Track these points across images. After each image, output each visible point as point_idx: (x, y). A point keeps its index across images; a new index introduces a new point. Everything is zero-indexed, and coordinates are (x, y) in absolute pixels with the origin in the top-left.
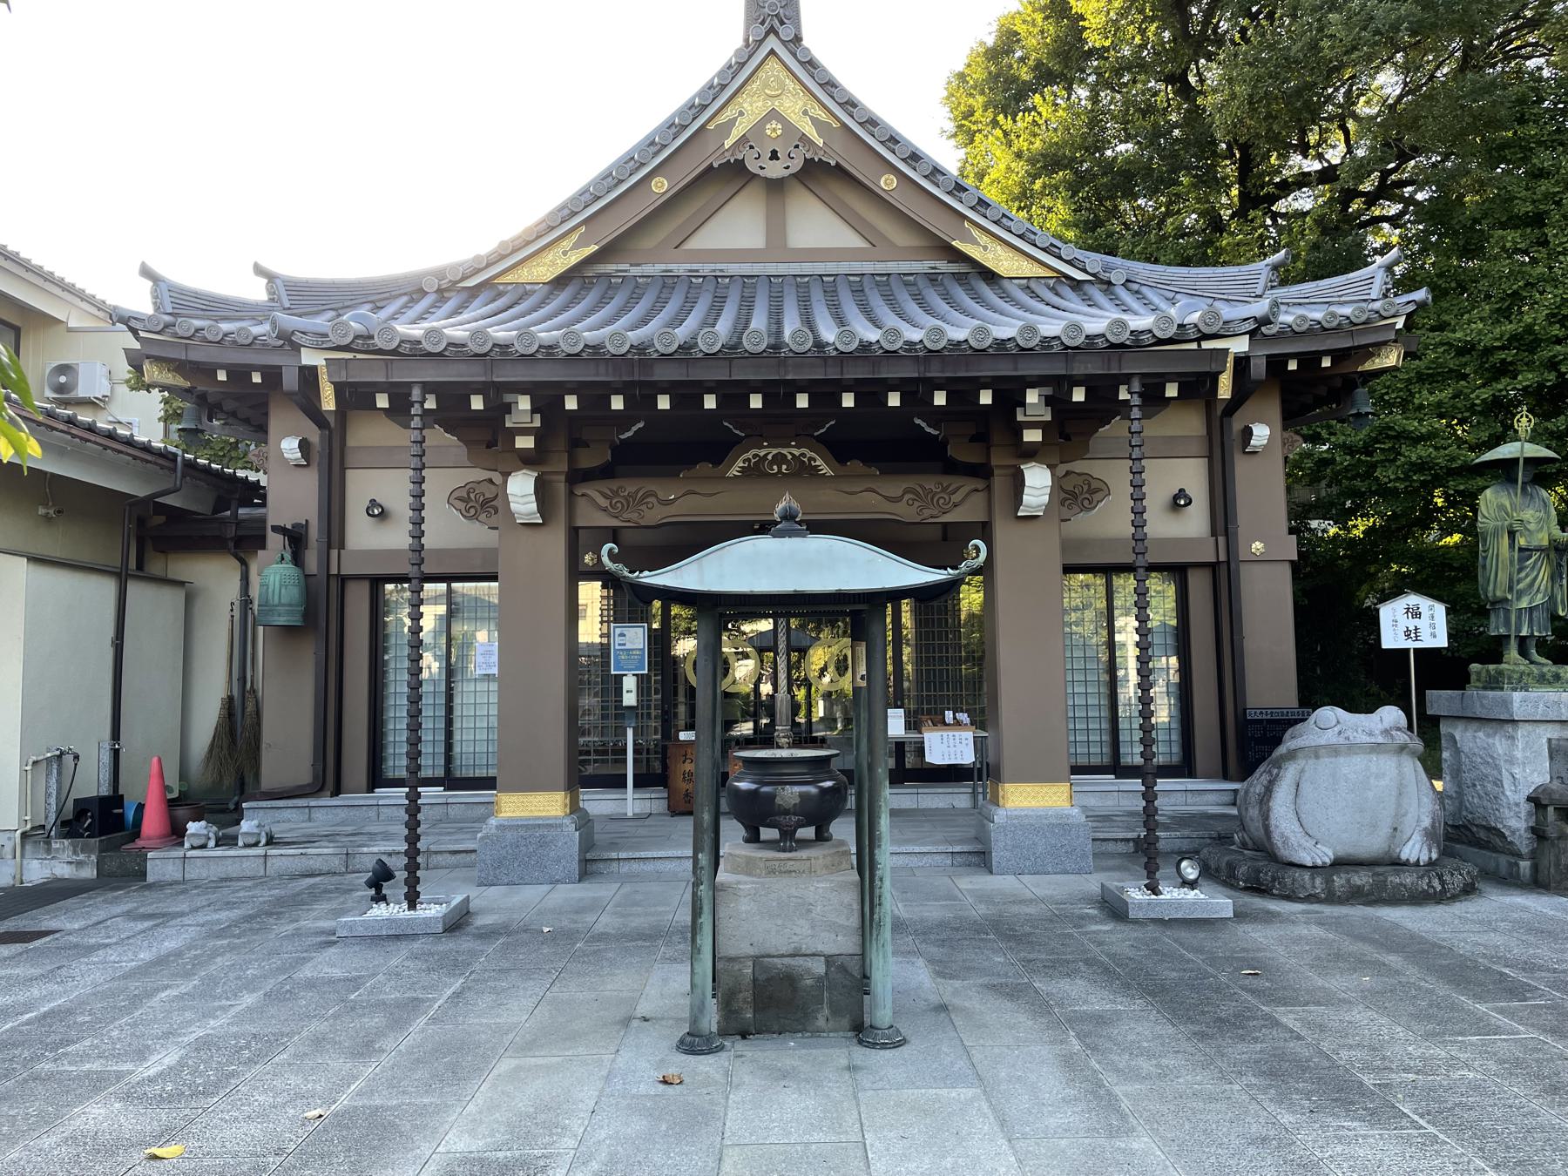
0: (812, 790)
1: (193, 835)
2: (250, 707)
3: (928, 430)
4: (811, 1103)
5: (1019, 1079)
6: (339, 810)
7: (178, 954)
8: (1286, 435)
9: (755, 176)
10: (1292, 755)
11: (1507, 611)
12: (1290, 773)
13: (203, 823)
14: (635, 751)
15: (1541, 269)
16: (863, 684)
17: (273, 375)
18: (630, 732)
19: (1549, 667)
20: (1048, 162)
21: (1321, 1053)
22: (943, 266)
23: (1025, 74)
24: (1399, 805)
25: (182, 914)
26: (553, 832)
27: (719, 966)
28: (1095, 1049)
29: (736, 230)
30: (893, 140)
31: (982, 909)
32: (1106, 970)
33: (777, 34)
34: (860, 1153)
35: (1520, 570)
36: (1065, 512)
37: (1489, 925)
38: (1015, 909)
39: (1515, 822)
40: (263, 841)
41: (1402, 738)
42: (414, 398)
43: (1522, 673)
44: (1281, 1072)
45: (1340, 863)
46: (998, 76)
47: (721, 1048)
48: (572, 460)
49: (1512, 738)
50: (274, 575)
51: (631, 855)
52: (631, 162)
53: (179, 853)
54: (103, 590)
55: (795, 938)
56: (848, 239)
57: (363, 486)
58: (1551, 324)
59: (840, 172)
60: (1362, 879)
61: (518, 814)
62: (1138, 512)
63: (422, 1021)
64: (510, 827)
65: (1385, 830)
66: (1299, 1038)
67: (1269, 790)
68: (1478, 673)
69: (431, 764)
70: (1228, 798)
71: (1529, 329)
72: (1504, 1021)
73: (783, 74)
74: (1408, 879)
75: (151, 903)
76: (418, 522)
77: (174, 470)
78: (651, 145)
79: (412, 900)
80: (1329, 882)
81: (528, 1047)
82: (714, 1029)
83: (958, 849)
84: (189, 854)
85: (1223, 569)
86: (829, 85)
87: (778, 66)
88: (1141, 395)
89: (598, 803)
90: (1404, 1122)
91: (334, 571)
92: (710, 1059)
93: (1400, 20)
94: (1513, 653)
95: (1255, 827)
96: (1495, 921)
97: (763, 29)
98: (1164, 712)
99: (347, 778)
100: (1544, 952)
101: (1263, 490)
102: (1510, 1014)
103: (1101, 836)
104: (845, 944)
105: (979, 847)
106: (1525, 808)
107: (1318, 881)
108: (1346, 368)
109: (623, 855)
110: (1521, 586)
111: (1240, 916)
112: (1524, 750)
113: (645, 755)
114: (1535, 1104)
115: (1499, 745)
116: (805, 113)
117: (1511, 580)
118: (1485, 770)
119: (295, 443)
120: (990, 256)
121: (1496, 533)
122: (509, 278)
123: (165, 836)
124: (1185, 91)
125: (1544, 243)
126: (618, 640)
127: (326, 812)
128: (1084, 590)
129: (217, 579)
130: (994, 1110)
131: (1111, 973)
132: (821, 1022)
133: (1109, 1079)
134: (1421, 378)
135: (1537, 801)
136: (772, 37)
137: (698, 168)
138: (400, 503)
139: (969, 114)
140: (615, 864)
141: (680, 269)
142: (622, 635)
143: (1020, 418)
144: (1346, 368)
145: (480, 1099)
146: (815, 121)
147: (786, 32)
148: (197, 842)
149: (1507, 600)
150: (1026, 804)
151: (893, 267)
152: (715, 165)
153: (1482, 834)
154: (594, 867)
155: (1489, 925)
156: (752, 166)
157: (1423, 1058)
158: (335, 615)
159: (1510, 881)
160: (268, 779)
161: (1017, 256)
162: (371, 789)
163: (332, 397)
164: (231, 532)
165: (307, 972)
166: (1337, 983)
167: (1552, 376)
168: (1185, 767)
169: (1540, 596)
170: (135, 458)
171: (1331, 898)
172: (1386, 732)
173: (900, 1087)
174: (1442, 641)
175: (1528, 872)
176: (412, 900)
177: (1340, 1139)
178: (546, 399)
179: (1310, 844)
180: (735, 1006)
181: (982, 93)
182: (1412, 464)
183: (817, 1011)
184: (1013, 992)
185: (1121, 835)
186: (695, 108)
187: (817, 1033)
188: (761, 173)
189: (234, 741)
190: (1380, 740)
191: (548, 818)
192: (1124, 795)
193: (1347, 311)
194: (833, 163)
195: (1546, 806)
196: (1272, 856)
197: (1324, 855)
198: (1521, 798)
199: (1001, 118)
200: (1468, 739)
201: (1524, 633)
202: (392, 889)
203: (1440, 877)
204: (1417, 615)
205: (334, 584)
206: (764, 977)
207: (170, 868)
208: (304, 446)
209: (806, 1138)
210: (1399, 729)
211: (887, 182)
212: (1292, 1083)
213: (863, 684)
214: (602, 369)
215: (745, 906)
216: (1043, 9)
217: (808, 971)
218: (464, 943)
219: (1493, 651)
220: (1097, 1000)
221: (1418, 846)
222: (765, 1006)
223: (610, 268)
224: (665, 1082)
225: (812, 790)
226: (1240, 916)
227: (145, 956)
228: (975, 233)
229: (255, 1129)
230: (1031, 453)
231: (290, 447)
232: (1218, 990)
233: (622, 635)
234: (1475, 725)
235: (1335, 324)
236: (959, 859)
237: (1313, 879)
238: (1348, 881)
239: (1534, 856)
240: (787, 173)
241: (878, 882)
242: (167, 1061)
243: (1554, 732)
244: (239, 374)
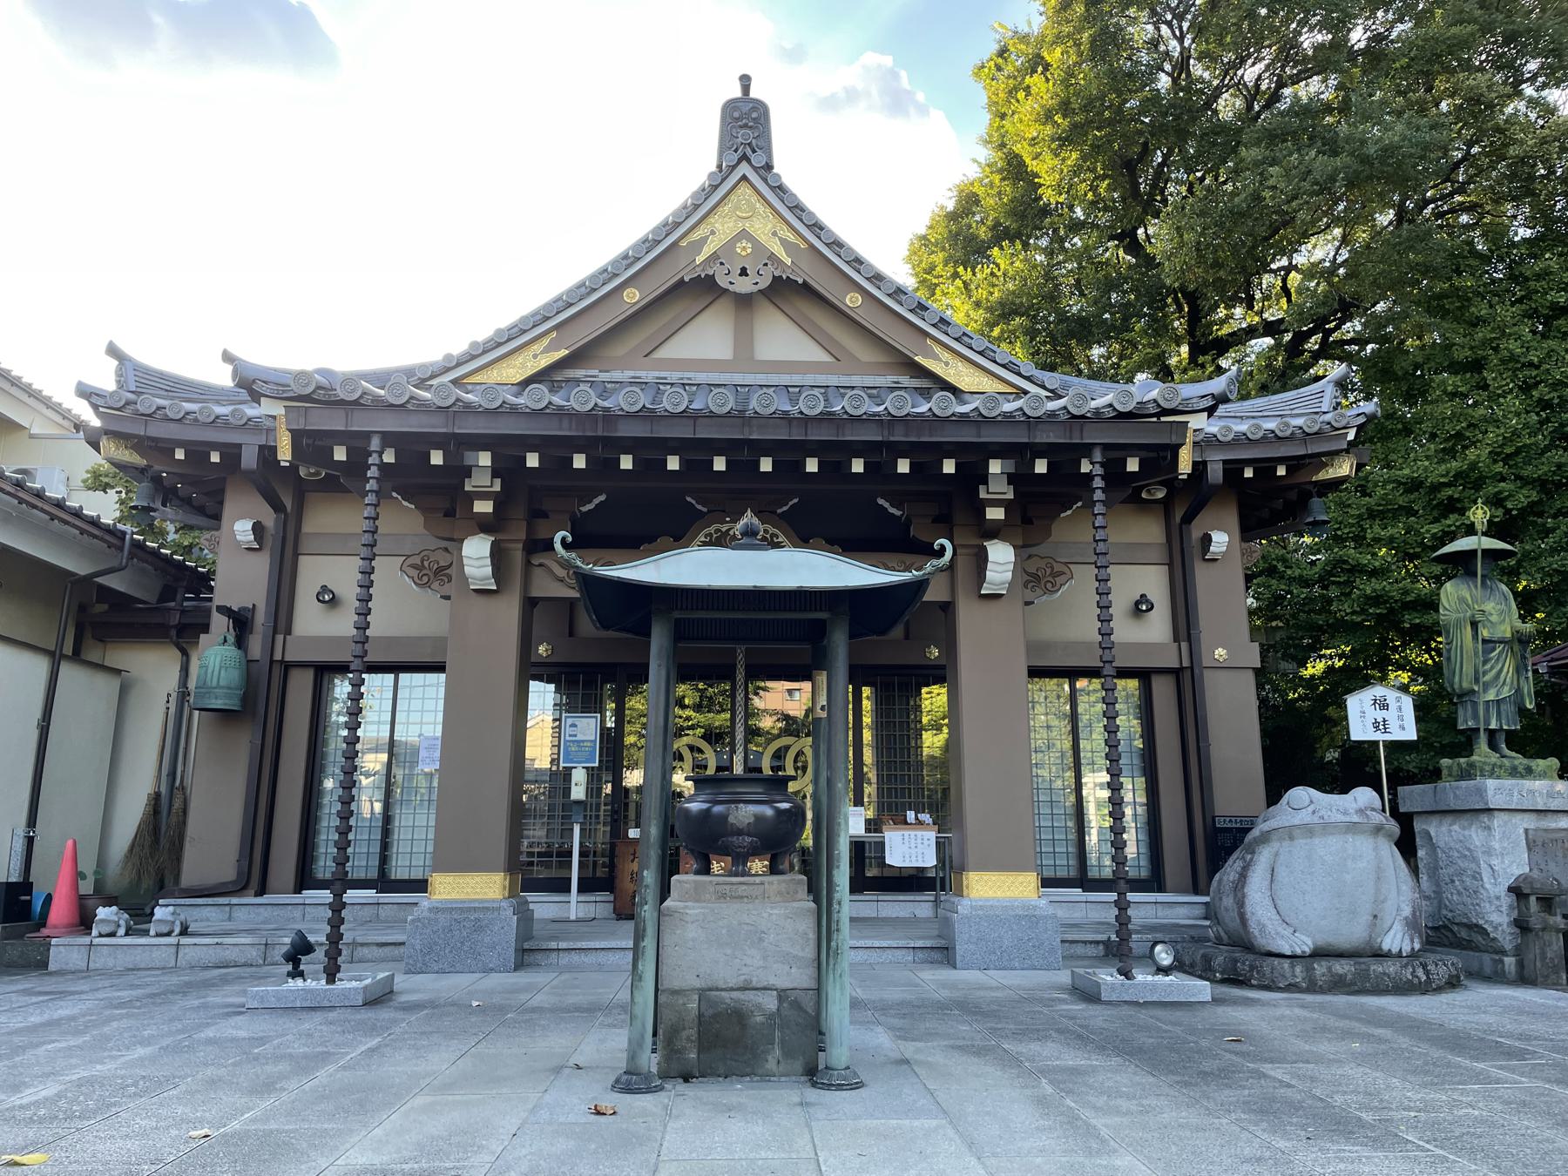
0: (768, 811)
1: (102, 921)
2: (177, 804)
3: (892, 510)
4: (758, 1129)
5: (988, 1113)
6: (262, 909)
7: (73, 1018)
8: (1245, 545)
9: (727, 290)
10: (1265, 838)
11: (1475, 704)
12: (1264, 856)
13: (114, 908)
14: (581, 855)
15: (1481, 411)
16: (824, 715)
17: (232, 454)
18: (577, 829)
19: (1520, 760)
20: (1005, 311)
21: (1314, 1097)
22: (906, 381)
23: (983, 233)
24: (1378, 890)
25: (82, 992)
26: (489, 915)
27: (662, 999)
28: (1069, 1092)
29: (704, 342)
30: (857, 262)
31: (945, 993)
32: (1080, 1037)
33: (749, 161)
34: (813, 1166)
35: (1485, 663)
36: (1029, 596)
37: (1479, 1009)
38: (982, 993)
39: (1497, 916)
40: (177, 930)
41: (1378, 818)
42: (373, 448)
43: (1494, 765)
44: (1270, 1110)
45: (1319, 954)
46: (958, 234)
47: (660, 1089)
48: (530, 529)
49: (1489, 828)
50: (216, 658)
51: (571, 945)
52: (606, 274)
53: (86, 940)
54: (38, 667)
55: (745, 970)
56: (811, 352)
57: (314, 572)
58: (1495, 462)
59: (807, 290)
60: (1342, 967)
61: (454, 896)
62: (1105, 619)
63: (331, 1068)
64: (444, 910)
65: (1365, 918)
66: (1289, 1086)
67: (1243, 876)
68: (1450, 768)
69: (362, 862)
70: (1200, 911)
71: (1473, 466)
72: (1503, 1074)
73: (755, 198)
74: (1391, 968)
75: (49, 984)
76: (365, 613)
77: (121, 549)
78: (626, 259)
79: (331, 974)
80: (1309, 970)
81: (447, 1087)
82: (654, 1070)
83: (920, 944)
84: (96, 941)
85: (1188, 674)
86: (798, 208)
87: (749, 191)
88: (1102, 465)
89: (544, 906)
90: (1409, 1146)
91: (278, 657)
92: (648, 1097)
93: (1336, 171)
94: (1482, 744)
95: (1231, 919)
96: (1482, 1006)
97: (736, 156)
98: (1133, 846)
99: (272, 880)
100: (1539, 1027)
101: (1227, 602)
102: (1512, 1070)
103: (1069, 937)
104: (798, 977)
105: (942, 943)
106: (1507, 900)
107: (1298, 969)
108: (1301, 478)
109: (563, 945)
110: (1487, 678)
111: (1216, 1001)
112: (1501, 840)
113: (591, 858)
114: (1548, 1133)
115: (1474, 835)
116: (774, 234)
117: (1476, 672)
118: (1462, 864)
119: (248, 525)
120: (952, 372)
121: (1459, 624)
122: (476, 379)
123: (73, 925)
124: (1134, 247)
125: (1485, 387)
126: (569, 731)
127: (249, 910)
128: (1048, 697)
129: (155, 671)
130: (961, 1136)
131: (1081, 1038)
132: (771, 1064)
133: (1086, 1114)
134: (1372, 514)
135: (1518, 892)
136: (744, 163)
137: (670, 283)
138: (348, 590)
139: (930, 269)
140: (554, 955)
141: (649, 376)
142: (573, 725)
143: (983, 495)
144: (1301, 478)
145: (387, 1125)
146: (784, 242)
147: (758, 159)
148: (106, 929)
149: (1473, 691)
150: (991, 894)
151: (856, 380)
152: (687, 279)
153: (1464, 934)
154: (528, 958)
155: (1479, 1009)
156: (722, 282)
157: (1422, 1100)
158: (277, 709)
159: (1496, 977)
160: (188, 878)
161: (978, 373)
162: (298, 890)
163: (289, 447)
164: (175, 619)
165: (210, 1033)
166: (1325, 1047)
167: (1500, 512)
168: (1155, 882)
169: (1506, 688)
170: (82, 532)
171: (1312, 988)
172: (1361, 811)
173: (856, 1118)
174: (1411, 734)
175: (1513, 968)
176: (331, 974)
177: (1342, 1160)
178: (507, 452)
179: (1287, 932)
180: (678, 1045)
181: (943, 249)
182: (1367, 597)
183: (767, 1052)
184: (980, 1052)
185: (1090, 937)
186: (669, 227)
187: (766, 1076)
188: (731, 288)
189: (156, 841)
190: (1356, 819)
191: (482, 901)
192: (1097, 909)
193: (1299, 422)
194: (800, 281)
195: (1527, 895)
196: (1248, 947)
197: (1304, 944)
198: (1501, 890)
199: (961, 269)
200: (1439, 833)
201: (1493, 726)
202: (310, 964)
203: (1424, 966)
204: (1385, 706)
205: (277, 672)
206: (711, 1012)
207: (75, 955)
208: (258, 529)
209: (751, 1156)
210: (1373, 809)
211: (852, 300)
212: (1285, 1118)
213: (824, 715)
214: (565, 423)
215: (692, 932)
216: (1000, 171)
217: (759, 1006)
218: (383, 1014)
219: (1463, 744)
220: (1072, 1058)
221: (1399, 936)
222: (709, 1045)
223: (579, 373)
224: (598, 1113)
225: (768, 811)
226: (1216, 1001)
227: (35, 1019)
228: (937, 349)
229: (133, 1145)
230: (995, 532)
231: (243, 529)
232: (1199, 1052)
233: (573, 725)
234: (1449, 819)
235: (1288, 433)
236: (920, 955)
237: (1293, 967)
238: (1329, 969)
239: (1518, 952)
240: (755, 289)
241: (836, 906)
242: (44, 1093)
243: (1530, 822)
244: (197, 452)
